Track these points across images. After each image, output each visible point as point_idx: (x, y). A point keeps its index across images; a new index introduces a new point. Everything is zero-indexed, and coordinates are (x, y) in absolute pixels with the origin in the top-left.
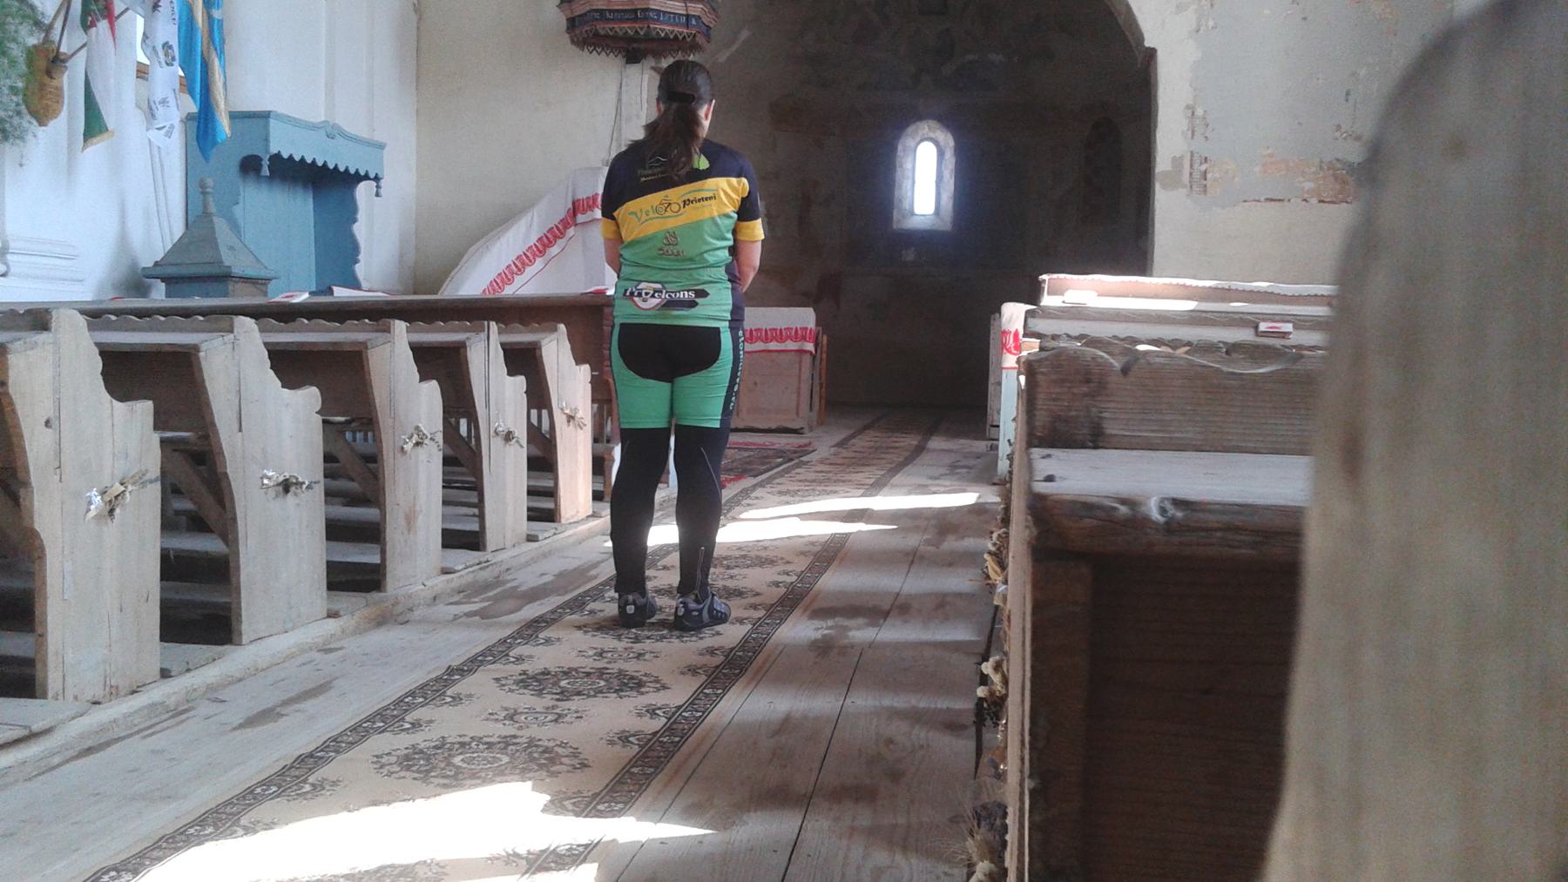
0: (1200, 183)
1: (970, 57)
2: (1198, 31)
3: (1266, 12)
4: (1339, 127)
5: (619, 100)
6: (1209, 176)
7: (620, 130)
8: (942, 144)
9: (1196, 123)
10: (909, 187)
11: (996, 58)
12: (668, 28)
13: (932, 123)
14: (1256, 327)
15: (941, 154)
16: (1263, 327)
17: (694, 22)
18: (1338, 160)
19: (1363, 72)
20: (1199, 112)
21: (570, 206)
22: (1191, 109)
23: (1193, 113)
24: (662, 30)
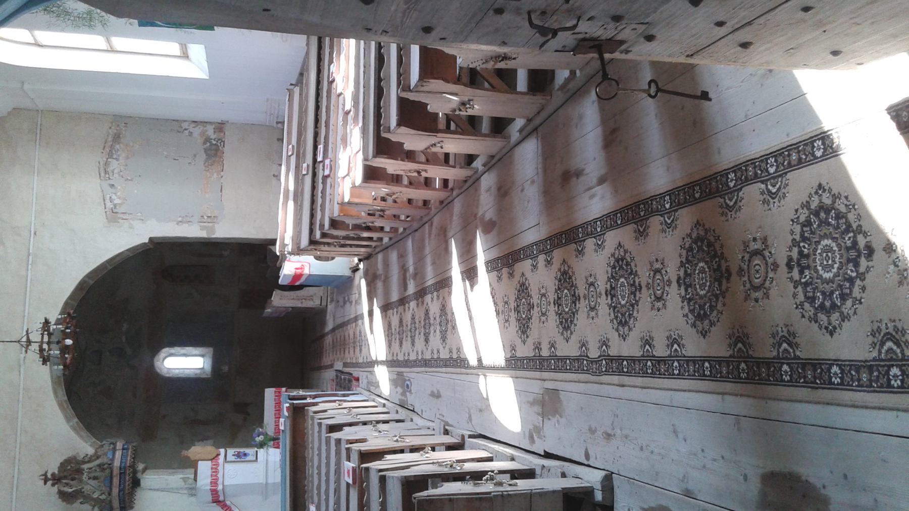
0: (212, 219)
1: (124, 340)
2: (143, 220)
3: (136, 191)
4: (189, 163)
5: (158, 490)
6: (209, 215)
7: (172, 488)
8: (166, 355)
9: (184, 220)
10: (188, 371)
11: (125, 326)
12: (129, 458)
13: (156, 359)
14: (304, 175)
15: (171, 355)
16: (304, 172)
17: (126, 446)
18: (204, 164)
19: (165, 153)
20: (180, 219)
21: (215, 504)
22: (179, 223)
23: (180, 222)
24: (130, 460)
